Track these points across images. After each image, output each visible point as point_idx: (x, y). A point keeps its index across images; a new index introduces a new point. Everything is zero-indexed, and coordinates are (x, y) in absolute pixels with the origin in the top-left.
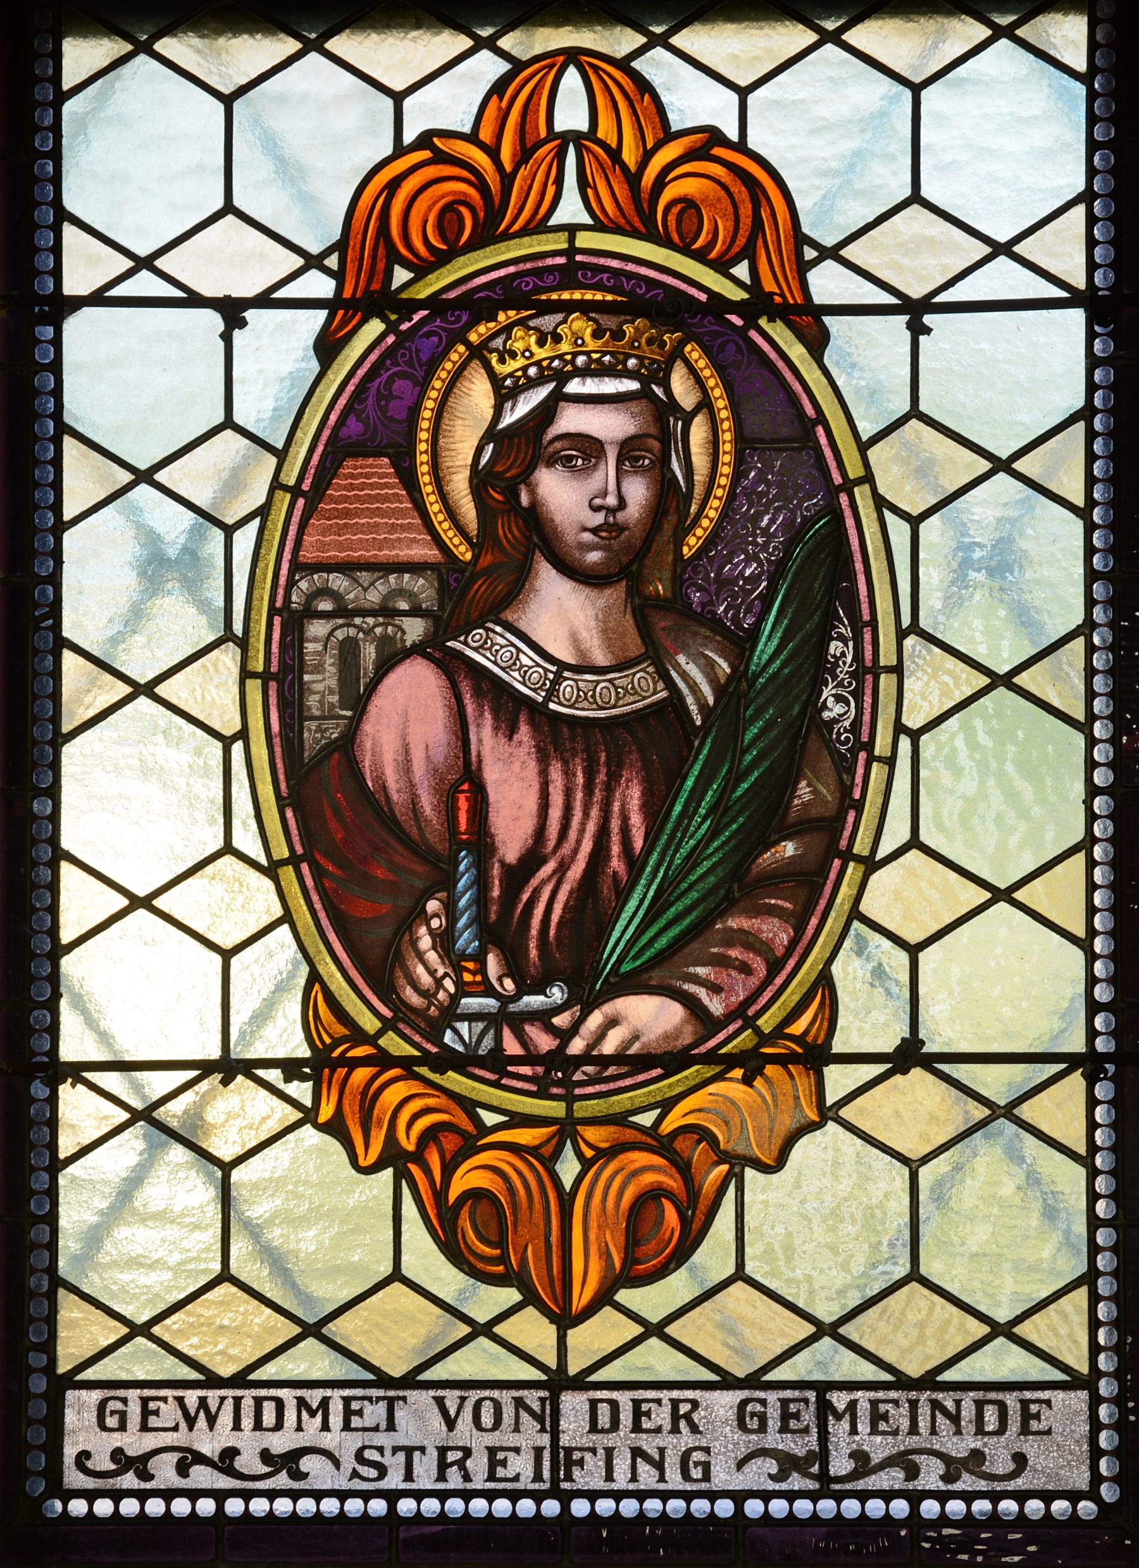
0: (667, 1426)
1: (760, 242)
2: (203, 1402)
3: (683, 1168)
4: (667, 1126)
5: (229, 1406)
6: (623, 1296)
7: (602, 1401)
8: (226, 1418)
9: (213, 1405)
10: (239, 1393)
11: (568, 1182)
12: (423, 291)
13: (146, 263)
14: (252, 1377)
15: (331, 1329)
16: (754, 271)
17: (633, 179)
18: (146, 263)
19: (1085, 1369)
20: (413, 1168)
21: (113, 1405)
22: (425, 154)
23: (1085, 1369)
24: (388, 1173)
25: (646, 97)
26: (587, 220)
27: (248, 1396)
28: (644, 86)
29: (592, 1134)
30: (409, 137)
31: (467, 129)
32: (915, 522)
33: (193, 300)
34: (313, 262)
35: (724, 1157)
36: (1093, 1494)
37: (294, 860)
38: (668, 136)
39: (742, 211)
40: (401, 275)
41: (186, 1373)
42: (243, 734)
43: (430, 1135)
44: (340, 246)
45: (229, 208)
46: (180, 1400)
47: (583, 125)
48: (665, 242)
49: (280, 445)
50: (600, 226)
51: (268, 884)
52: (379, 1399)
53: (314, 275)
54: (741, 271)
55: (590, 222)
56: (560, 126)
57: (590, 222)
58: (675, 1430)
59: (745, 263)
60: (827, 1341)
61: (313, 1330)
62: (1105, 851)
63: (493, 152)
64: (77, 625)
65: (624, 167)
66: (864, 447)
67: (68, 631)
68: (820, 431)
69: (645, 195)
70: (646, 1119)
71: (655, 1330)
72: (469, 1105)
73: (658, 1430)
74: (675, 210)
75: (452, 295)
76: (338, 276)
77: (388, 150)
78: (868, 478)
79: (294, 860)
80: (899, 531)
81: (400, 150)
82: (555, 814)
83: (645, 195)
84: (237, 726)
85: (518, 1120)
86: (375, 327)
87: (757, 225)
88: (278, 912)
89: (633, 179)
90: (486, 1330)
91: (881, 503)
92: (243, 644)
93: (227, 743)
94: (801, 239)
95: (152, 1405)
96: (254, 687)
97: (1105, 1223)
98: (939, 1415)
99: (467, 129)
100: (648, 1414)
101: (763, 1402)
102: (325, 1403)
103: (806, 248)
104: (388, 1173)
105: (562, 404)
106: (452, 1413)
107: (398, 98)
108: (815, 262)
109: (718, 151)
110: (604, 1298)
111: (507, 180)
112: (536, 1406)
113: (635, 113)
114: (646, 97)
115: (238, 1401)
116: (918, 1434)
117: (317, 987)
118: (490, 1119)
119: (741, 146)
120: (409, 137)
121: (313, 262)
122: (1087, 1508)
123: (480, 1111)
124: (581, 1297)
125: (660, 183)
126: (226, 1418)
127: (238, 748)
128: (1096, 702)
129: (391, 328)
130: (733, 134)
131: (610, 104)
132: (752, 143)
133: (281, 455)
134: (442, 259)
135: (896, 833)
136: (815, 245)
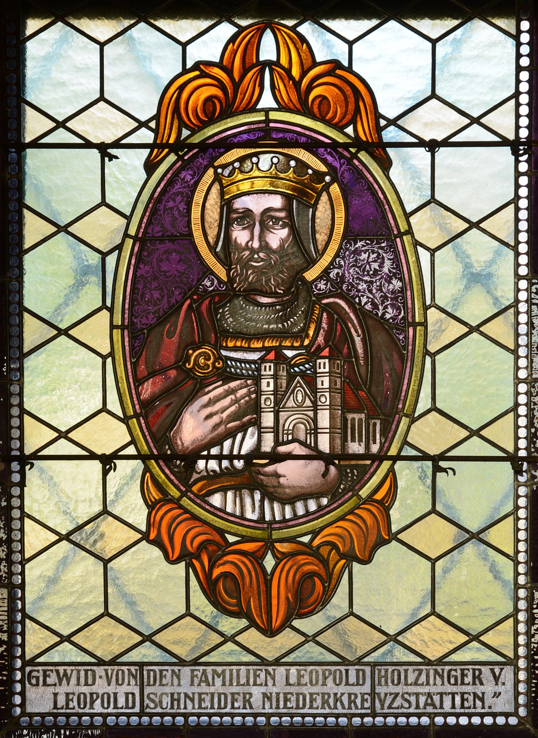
1: (358, 119)
3: (325, 562)
4: (316, 542)
5: (75, 673)
6: (296, 623)
8: (73, 681)
9: (69, 672)
11: (269, 570)
12: (197, 139)
13: (61, 124)
14: (119, 660)
15: (157, 638)
16: (355, 130)
17: (297, 84)
18: (61, 124)
19: (511, 655)
20: (194, 561)
21: (453, 673)
22: (197, 73)
23: (511, 655)
24: (183, 564)
25: (305, 45)
26: (275, 106)
28: (303, 39)
29: (283, 547)
30: (189, 65)
31: (217, 60)
32: (433, 252)
33: (88, 144)
34: (142, 124)
35: (342, 556)
36: (515, 714)
37: (136, 416)
38: (315, 64)
39: (350, 107)
40: (186, 133)
41: (88, 659)
42: (112, 354)
43: (203, 546)
44: (156, 117)
45: (102, 98)
46: (57, 672)
47: (274, 58)
48: (313, 117)
49: (128, 214)
50: (282, 108)
51: (124, 426)
53: (144, 130)
54: (350, 130)
55: (276, 106)
56: (262, 58)
57: (276, 106)
59: (352, 126)
60: (392, 632)
61: (148, 638)
63: (229, 71)
65: (291, 77)
66: (407, 216)
67: (28, 303)
70: (306, 539)
71: (313, 638)
72: (221, 532)
74: (318, 101)
75: (211, 141)
76: (156, 131)
77: (180, 70)
78: (410, 232)
79: (136, 416)
80: (424, 256)
81: (185, 71)
84: (109, 350)
85: (245, 539)
86: (172, 158)
87: (357, 110)
88: (128, 439)
89: (297, 84)
90: (232, 639)
91: (416, 244)
92: (111, 310)
93: (104, 358)
94: (378, 116)
95: (195, 673)
96: (117, 333)
97: (523, 587)
99: (217, 60)
102: (224, 672)
104: (183, 564)
106: (497, 674)
107: (184, 45)
108: (386, 127)
109: (338, 72)
110: (286, 624)
111: (236, 86)
112: (134, 672)
113: (297, 50)
114: (305, 45)
117: (148, 475)
118: (231, 539)
119: (349, 69)
120: (189, 65)
121: (142, 124)
122: (513, 721)
123: (227, 535)
124: (276, 623)
125: (310, 88)
126: (73, 681)
127: (109, 361)
129: (180, 158)
130: (346, 64)
131: (287, 52)
132: (355, 68)
133: (129, 218)
134: (205, 125)
135: (424, 404)
136: (384, 118)
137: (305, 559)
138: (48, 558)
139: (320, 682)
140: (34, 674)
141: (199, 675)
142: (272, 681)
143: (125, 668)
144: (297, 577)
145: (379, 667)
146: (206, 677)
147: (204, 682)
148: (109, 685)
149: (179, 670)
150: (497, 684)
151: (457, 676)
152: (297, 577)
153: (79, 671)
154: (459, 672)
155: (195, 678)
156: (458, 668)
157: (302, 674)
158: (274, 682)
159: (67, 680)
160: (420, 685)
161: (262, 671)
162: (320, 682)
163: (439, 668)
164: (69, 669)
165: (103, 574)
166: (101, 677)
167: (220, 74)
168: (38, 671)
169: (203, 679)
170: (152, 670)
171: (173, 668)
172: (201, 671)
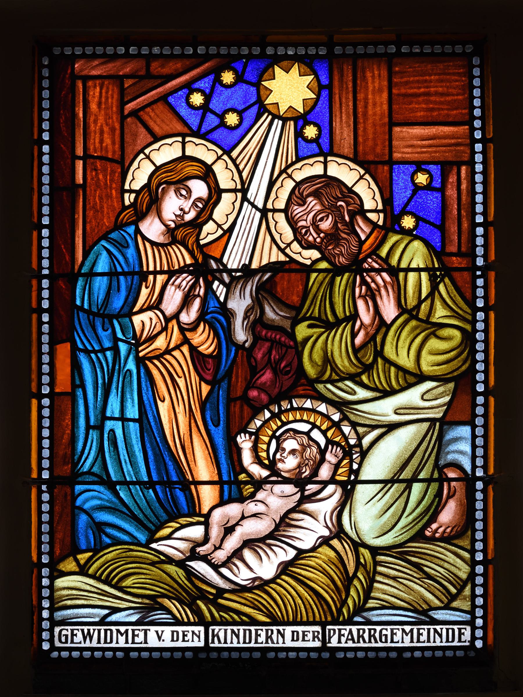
0: (311, 640)
2: (89, 630)
5: (96, 632)
10: (99, 627)
21: (64, 632)
27: (103, 628)
46: (83, 631)
52: (142, 630)
64: (357, 176)
73: (309, 641)
82: (370, 416)
95: (306, 633)
98: (237, 633)
100: (307, 635)
102: (127, 631)
122: (46, 646)
128: (477, 440)
140: (64, 632)
141: (346, 635)
143: (114, 628)
147: (350, 640)
149: (284, 630)
150: (160, 641)
153: (99, 631)
154: (389, 631)
155: (342, 637)
156: (389, 627)
157: (259, 634)
158: (284, 640)
163: (235, 628)
164: (91, 628)
167: (258, 139)
168: (67, 630)
169: (350, 637)
172: (348, 630)
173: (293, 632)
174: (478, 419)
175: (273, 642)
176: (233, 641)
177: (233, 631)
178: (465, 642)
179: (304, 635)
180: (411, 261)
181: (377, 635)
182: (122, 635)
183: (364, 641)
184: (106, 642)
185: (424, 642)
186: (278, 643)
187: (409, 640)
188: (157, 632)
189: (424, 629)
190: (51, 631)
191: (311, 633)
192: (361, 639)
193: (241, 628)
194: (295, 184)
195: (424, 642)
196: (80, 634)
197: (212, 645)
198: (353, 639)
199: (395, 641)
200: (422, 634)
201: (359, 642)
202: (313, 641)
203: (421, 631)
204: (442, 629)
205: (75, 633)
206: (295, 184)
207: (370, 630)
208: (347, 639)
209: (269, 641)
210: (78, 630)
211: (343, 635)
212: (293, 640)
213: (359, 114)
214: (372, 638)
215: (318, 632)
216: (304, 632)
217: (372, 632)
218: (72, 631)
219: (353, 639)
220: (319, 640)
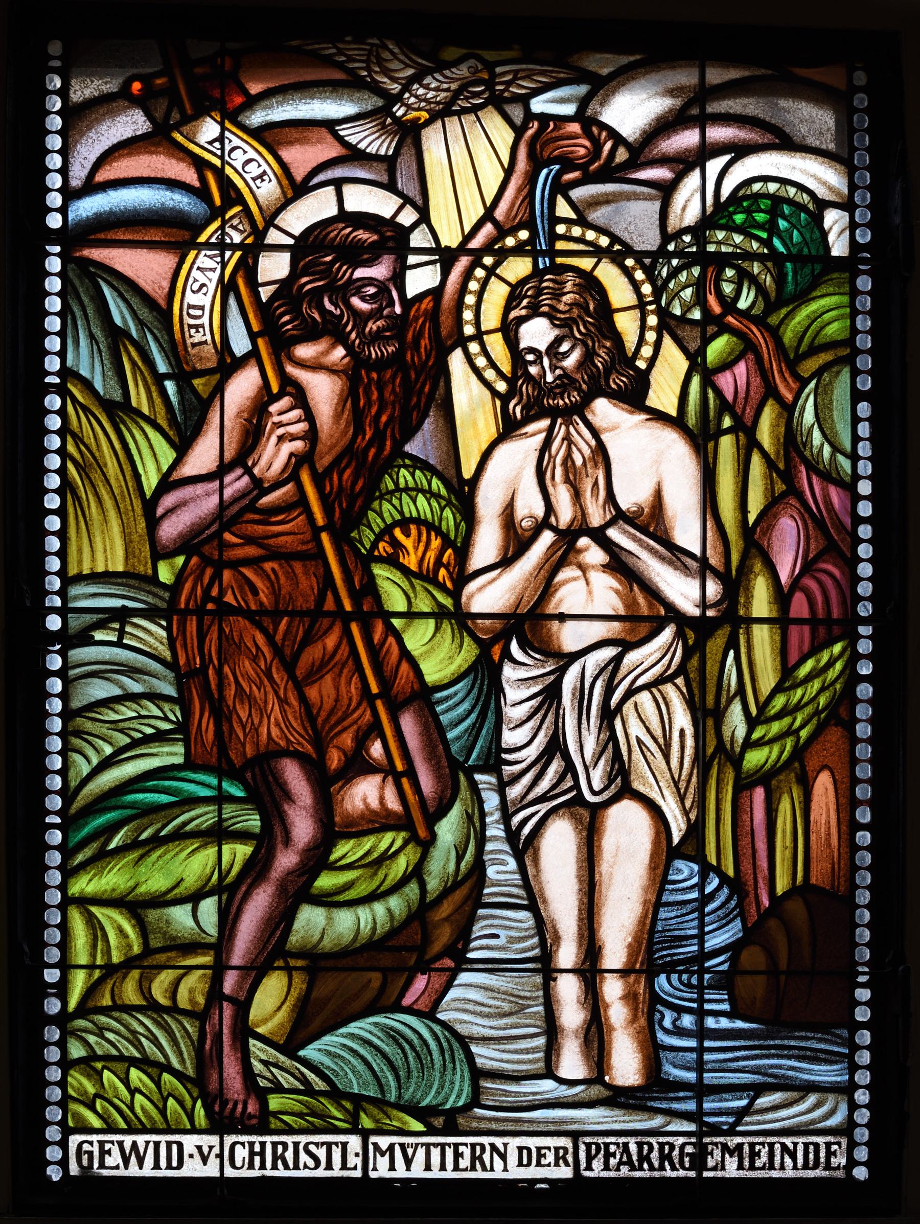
2: (134, 1145)
5: (151, 1146)
7: (612, 1143)
8: (149, 1160)
46: (121, 1144)
52: (323, 1144)
58: (557, 1164)
62: (52, 763)
68: (256, 328)
69: (83, 1035)
73: (549, 1165)
83: (83, 1035)
95: (543, 1152)
98: (502, 1151)
101: (91, 1143)
102: (391, 1147)
103: (196, 382)
105: (514, 283)
115: (157, 1145)
116: (446, 1170)
137: (784, 379)
138: (460, 174)
139: (534, 1162)
140: (86, 1147)
142: (502, 1163)
144: (310, 732)
145: (588, 1140)
146: (629, 1156)
147: (625, 1164)
148: (205, 1163)
151: (92, 1152)
152: (310, 732)
159: (791, 1157)
160: (544, 1166)
161: (764, 1147)
162: (534, 1162)
165: (800, 617)
166: (191, 1156)
169: (625, 1159)
170: (478, 1144)
171: (492, 1139)
173: (520, 1149)
174: (860, 767)
175: (484, 1169)
176: (397, 1166)
177: (784, 1147)
178: (838, 1168)
179: (540, 1156)
180: (93, 556)
181: (289, 1155)
182: (383, 1154)
183: (286, 1167)
184: (169, 1167)
185: (466, 1170)
186: (492, 1169)
187: (735, 1166)
188: (199, 1148)
189: (466, 1145)
190: (63, 1144)
191: (553, 1150)
192: (279, 1162)
193: (801, 1140)
194: (500, 334)
195: (466, 1170)
196: (115, 1150)
197: (587, 1174)
198: (630, 1163)
199: (348, 1166)
200: (462, 1155)
201: (662, 1168)
202: (555, 1166)
203: (107, 1146)
204: (795, 1144)
205: (833, 1150)
206: (500, 334)
207: (661, 1145)
208: (621, 1163)
209: (478, 1166)
210: (112, 1142)
211: (614, 1155)
212: (520, 1164)
213: (131, 296)
214: (477, 1163)
215: (566, 1149)
216: (539, 1149)
217: (280, 1149)
218: (101, 1143)
219: (630, 1163)
220: (567, 1164)
